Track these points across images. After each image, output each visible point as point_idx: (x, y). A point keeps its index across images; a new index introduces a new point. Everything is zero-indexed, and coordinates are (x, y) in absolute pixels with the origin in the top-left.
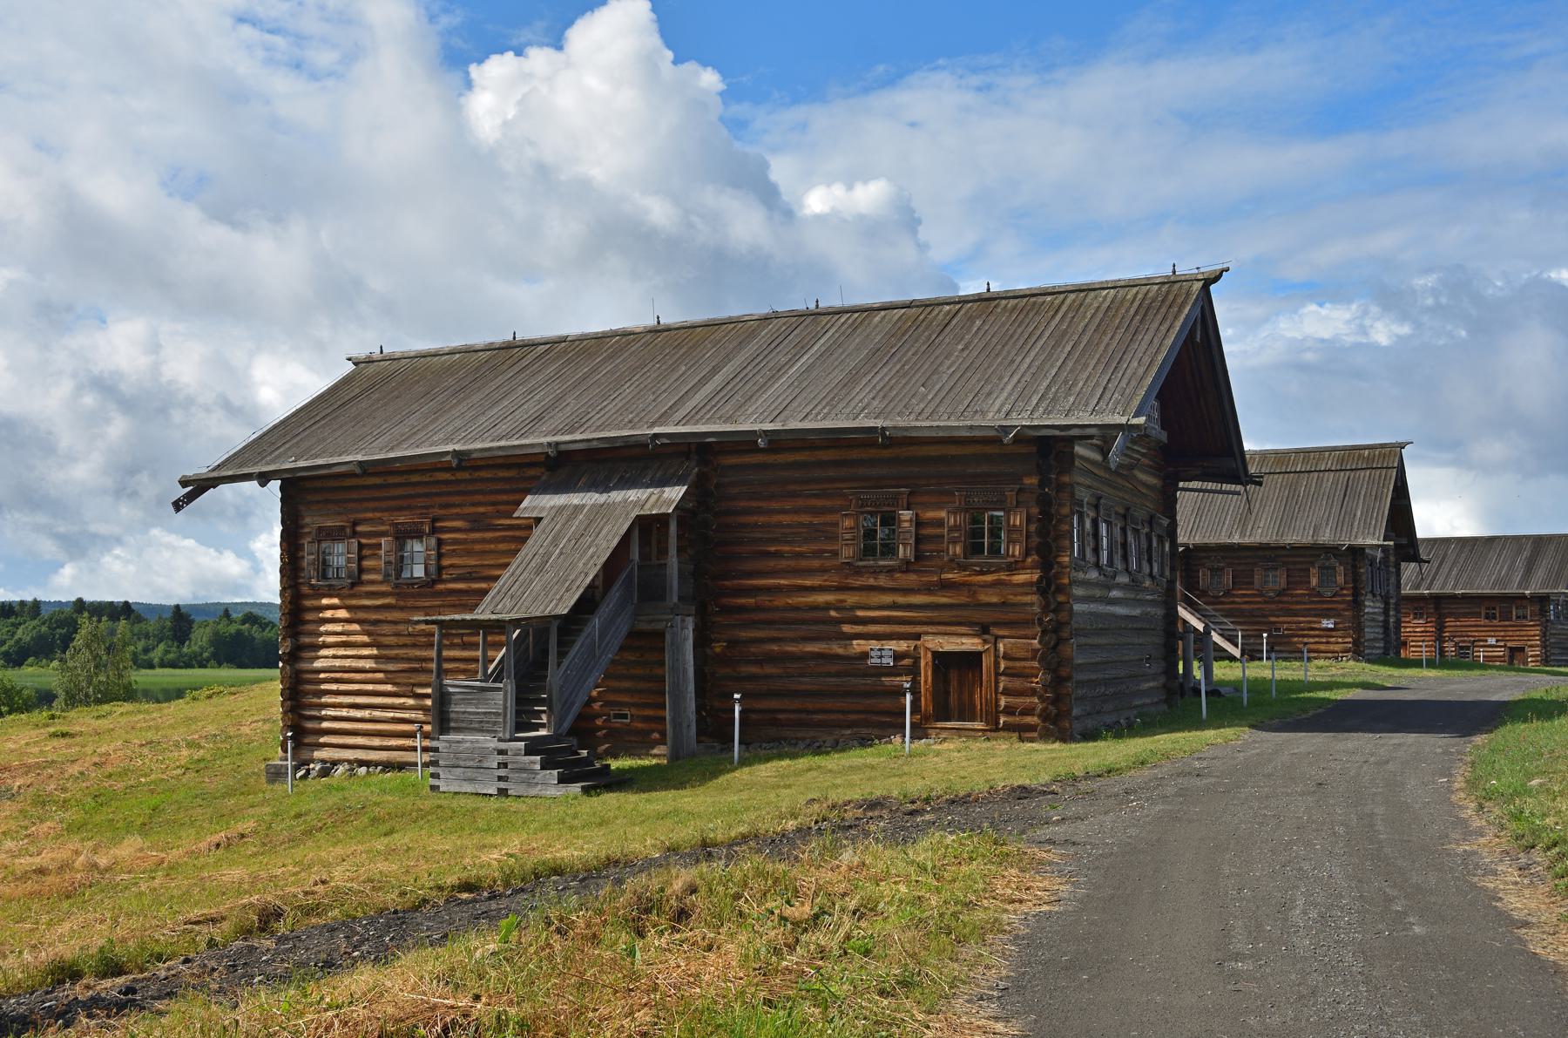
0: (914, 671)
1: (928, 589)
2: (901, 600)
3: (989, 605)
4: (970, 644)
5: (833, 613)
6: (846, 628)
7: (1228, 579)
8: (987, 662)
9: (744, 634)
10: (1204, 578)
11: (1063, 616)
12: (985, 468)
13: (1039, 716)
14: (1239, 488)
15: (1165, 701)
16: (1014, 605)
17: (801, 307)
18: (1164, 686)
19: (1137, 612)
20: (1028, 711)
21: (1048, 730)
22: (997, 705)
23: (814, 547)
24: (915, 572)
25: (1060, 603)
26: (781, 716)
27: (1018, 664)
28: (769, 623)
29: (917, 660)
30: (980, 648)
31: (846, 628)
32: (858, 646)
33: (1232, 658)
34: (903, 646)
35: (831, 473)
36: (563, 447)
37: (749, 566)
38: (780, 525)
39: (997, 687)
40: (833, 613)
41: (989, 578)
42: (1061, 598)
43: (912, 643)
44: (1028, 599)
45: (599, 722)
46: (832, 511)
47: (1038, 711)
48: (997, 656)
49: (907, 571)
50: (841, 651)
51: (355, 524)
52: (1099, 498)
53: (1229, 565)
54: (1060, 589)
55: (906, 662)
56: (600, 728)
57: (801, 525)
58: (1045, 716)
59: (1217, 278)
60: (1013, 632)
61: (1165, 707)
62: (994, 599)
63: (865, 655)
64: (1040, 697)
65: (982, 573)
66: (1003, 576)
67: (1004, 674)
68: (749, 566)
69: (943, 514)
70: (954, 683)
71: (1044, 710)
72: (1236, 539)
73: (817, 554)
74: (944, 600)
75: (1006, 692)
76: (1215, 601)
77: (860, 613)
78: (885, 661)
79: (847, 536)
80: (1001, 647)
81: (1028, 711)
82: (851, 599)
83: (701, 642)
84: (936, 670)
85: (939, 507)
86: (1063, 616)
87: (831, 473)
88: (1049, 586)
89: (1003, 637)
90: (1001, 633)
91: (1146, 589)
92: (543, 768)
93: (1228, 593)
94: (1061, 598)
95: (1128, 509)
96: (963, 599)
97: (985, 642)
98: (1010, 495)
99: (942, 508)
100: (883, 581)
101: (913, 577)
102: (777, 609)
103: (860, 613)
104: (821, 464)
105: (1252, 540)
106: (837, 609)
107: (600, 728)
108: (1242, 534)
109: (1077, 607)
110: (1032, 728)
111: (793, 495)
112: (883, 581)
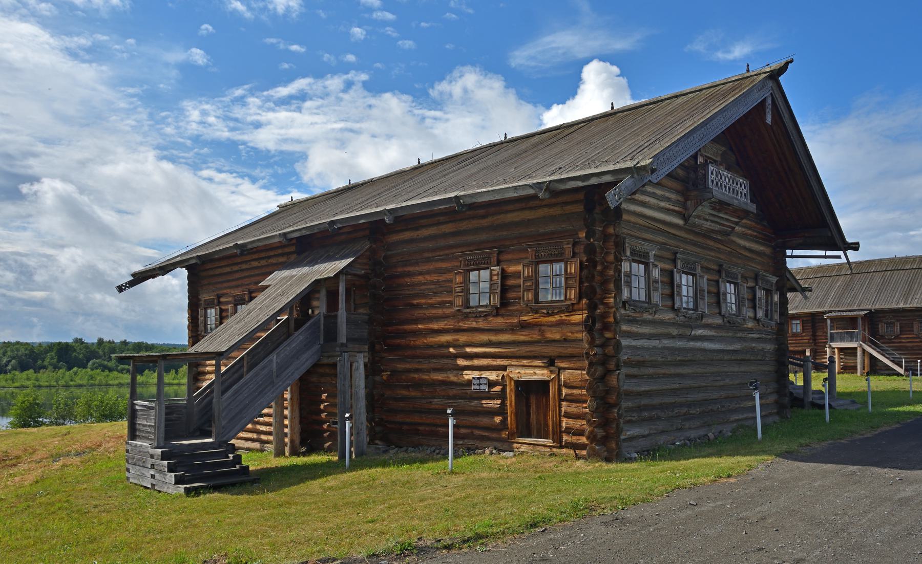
0: (502, 395)
1: (512, 329)
2: (493, 338)
3: (554, 341)
4: (541, 374)
5: (451, 350)
6: (461, 362)
7: (897, 329)
8: (553, 389)
9: (400, 366)
10: (882, 329)
11: (610, 350)
12: (551, 228)
13: (588, 438)
14: (840, 253)
15: (778, 413)
16: (574, 341)
17: (498, 140)
18: (776, 402)
19: (737, 346)
20: (580, 433)
21: (594, 450)
22: (561, 426)
23: (439, 299)
24: (502, 316)
25: (608, 339)
26: (421, 428)
27: (575, 391)
28: (414, 357)
29: (504, 390)
30: (545, 378)
31: (461, 362)
32: (468, 375)
33: (899, 374)
34: (492, 376)
35: (451, 241)
36: (290, 236)
37: (418, 313)
38: (420, 284)
39: (560, 411)
40: (451, 350)
41: (554, 319)
42: (608, 335)
43: (501, 373)
44: (580, 336)
45: (325, 426)
46: (449, 270)
47: (587, 433)
48: (560, 386)
49: (497, 315)
50: (455, 379)
51: (219, 297)
52: (675, 253)
53: (898, 321)
54: (606, 327)
55: (498, 388)
56: (326, 431)
57: (433, 283)
58: (592, 437)
59: (783, 69)
60: (571, 365)
61: (777, 418)
62: (558, 337)
63: (469, 383)
64: (588, 421)
65: (548, 315)
66: (563, 317)
67: (565, 400)
68: (418, 313)
69: (520, 268)
70: (533, 407)
71: (591, 432)
72: (901, 305)
73: (442, 304)
74: (522, 338)
75: (568, 415)
76: (890, 341)
77: (468, 350)
78: (482, 387)
79: (458, 290)
80: (562, 377)
81: (580, 433)
82: (462, 338)
83: (372, 370)
84: (518, 395)
85: (517, 261)
86: (610, 350)
87: (451, 241)
88: (594, 324)
89: (565, 369)
90: (562, 365)
91: (751, 330)
92: (275, 456)
93: (897, 337)
94: (608, 335)
95: (721, 266)
96: (536, 336)
97: (551, 372)
98: (568, 248)
99: (519, 263)
100: (481, 324)
101: (500, 320)
102: (419, 347)
103: (468, 350)
104: (444, 236)
105: (911, 305)
106: (454, 347)
107: (326, 431)
108: (905, 303)
109: (624, 342)
110: (582, 447)
111: (428, 260)
112: (481, 324)
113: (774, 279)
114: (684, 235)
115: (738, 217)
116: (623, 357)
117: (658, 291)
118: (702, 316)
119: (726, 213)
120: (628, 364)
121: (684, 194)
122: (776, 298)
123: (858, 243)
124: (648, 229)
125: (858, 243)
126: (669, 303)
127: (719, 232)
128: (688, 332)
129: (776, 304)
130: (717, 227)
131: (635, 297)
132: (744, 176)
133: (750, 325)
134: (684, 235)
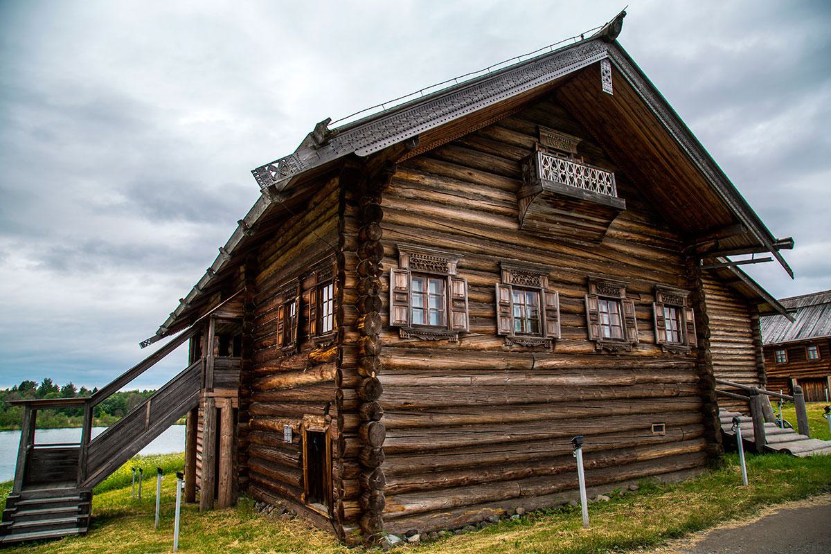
18: (703, 450)
113: (685, 294)
114: (515, 240)
115: (604, 216)
116: (383, 399)
117: (634, 327)
118: (555, 341)
119: (578, 212)
120: (390, 410)
121: (516, 192)
122: (690, 316)
123: (790, 240)
124: (444, 233)
125: (790, 240)
126: (584, 335)
127: (577, 237)
128: (527, 363)
129: (690, 324)
130: (576, 231)
131: (417, 320)
132: (606, 167)
133: (645, 351)
134: (515, 240)
